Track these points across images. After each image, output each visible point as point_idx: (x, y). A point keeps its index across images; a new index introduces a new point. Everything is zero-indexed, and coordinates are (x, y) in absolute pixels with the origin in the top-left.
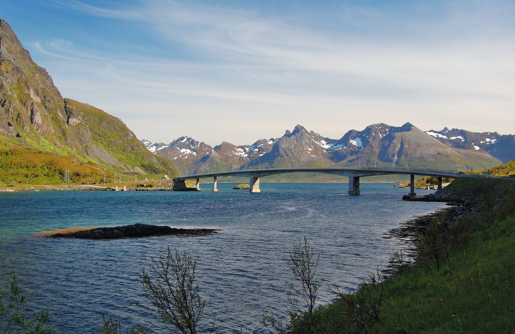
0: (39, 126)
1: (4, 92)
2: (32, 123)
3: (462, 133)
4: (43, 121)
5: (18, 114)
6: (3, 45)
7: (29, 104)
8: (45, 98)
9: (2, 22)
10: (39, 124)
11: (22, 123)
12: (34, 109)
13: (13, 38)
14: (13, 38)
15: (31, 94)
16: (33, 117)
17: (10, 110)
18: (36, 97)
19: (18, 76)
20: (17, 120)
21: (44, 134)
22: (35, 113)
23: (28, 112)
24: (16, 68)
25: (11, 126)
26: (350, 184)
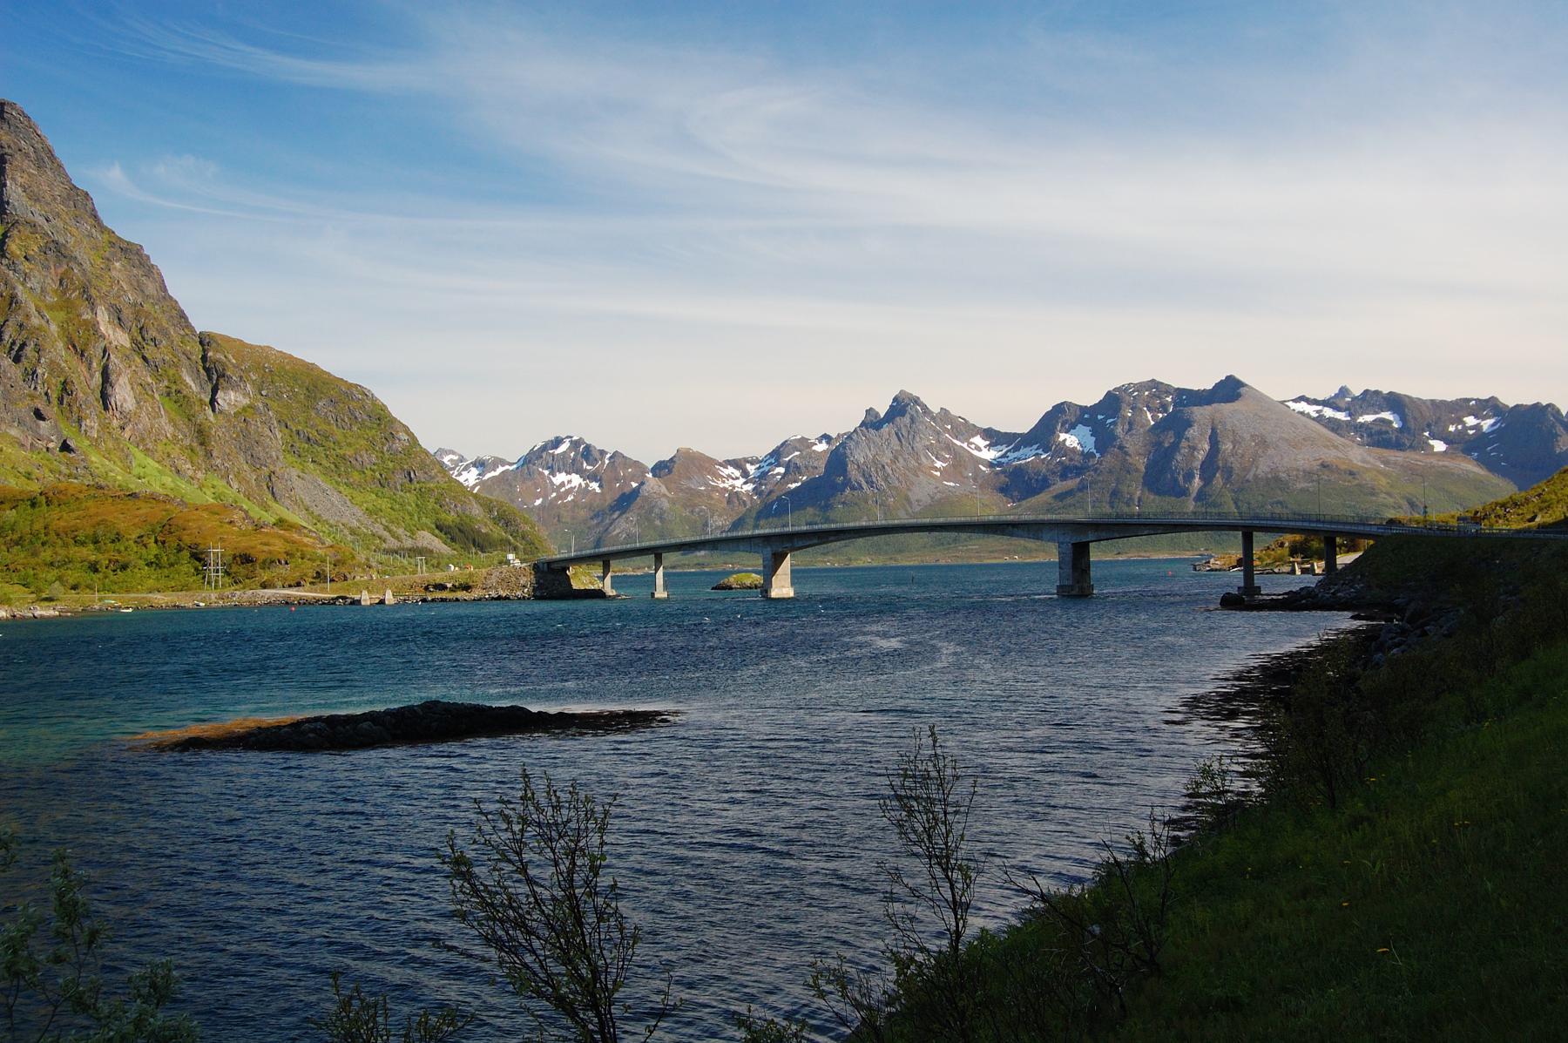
0: (126, 418)
1: (20, 318)
3: (1394, 402)
5: (65, 383)
6: (13, 179)
7: (95, 351)
8: (144, 333)
9: (7, 108)
10: (127, 410)
11: (75, 409)
12: (110, 367)
16: (109, 390)
17: (39, 371)
18: (114, 331)
19: (61, 270)
20: (61, 401)
22: (113, 377)
23: (92, 376)
24: (52, 246)
25: (44, 419)
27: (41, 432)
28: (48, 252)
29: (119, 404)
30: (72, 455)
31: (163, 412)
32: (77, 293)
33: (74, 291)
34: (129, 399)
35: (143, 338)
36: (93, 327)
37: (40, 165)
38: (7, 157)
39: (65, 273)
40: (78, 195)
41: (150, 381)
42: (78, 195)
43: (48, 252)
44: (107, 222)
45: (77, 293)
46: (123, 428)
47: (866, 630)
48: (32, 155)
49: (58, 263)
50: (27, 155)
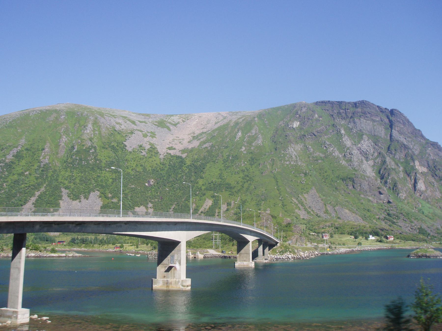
0: (422, 193)
1: (385, 167)
2: (415, 190)
3: (400, 112)
4: (426, 188)
5: (395, 183)
6: (395, 129)
7: (413, 175)
8: (436, 167)
9: (394, 111)
10: (422, 190)
11: (397, 191)
12: (417, 178)
13: (405, 121)
14: (405, 121)
15: (416, 165)
16: (416, 184)
17: (388, 181)
18: (421, 167)
19: (405, 152)
20: (393, 189)
21: (427, 199)
22: (417, 181)
23: (411, 181)
24: (403, 146)
25: (382, 194)
26: (244, 265)
27: (381, 198)
28: (402, 148)
29: (419, 188)
30: (391, 204)
31: (437, 190)
32: (410, 158)
33: (409, 157)
34: (423, 187)
35: (436, 169)
36: (413, 168)
37: (404, 124)
38: (393, 124)
39: (407, 153)
40: (416, 131)
41: (433, 181)
42: (416, 131)
43: (402, 148)
44: (427, 137)
45: (410, 158)
46: (421, 196)
47: (34, 258)
48: (401, 122)
49: (405, 150)
50: (400, 122)
